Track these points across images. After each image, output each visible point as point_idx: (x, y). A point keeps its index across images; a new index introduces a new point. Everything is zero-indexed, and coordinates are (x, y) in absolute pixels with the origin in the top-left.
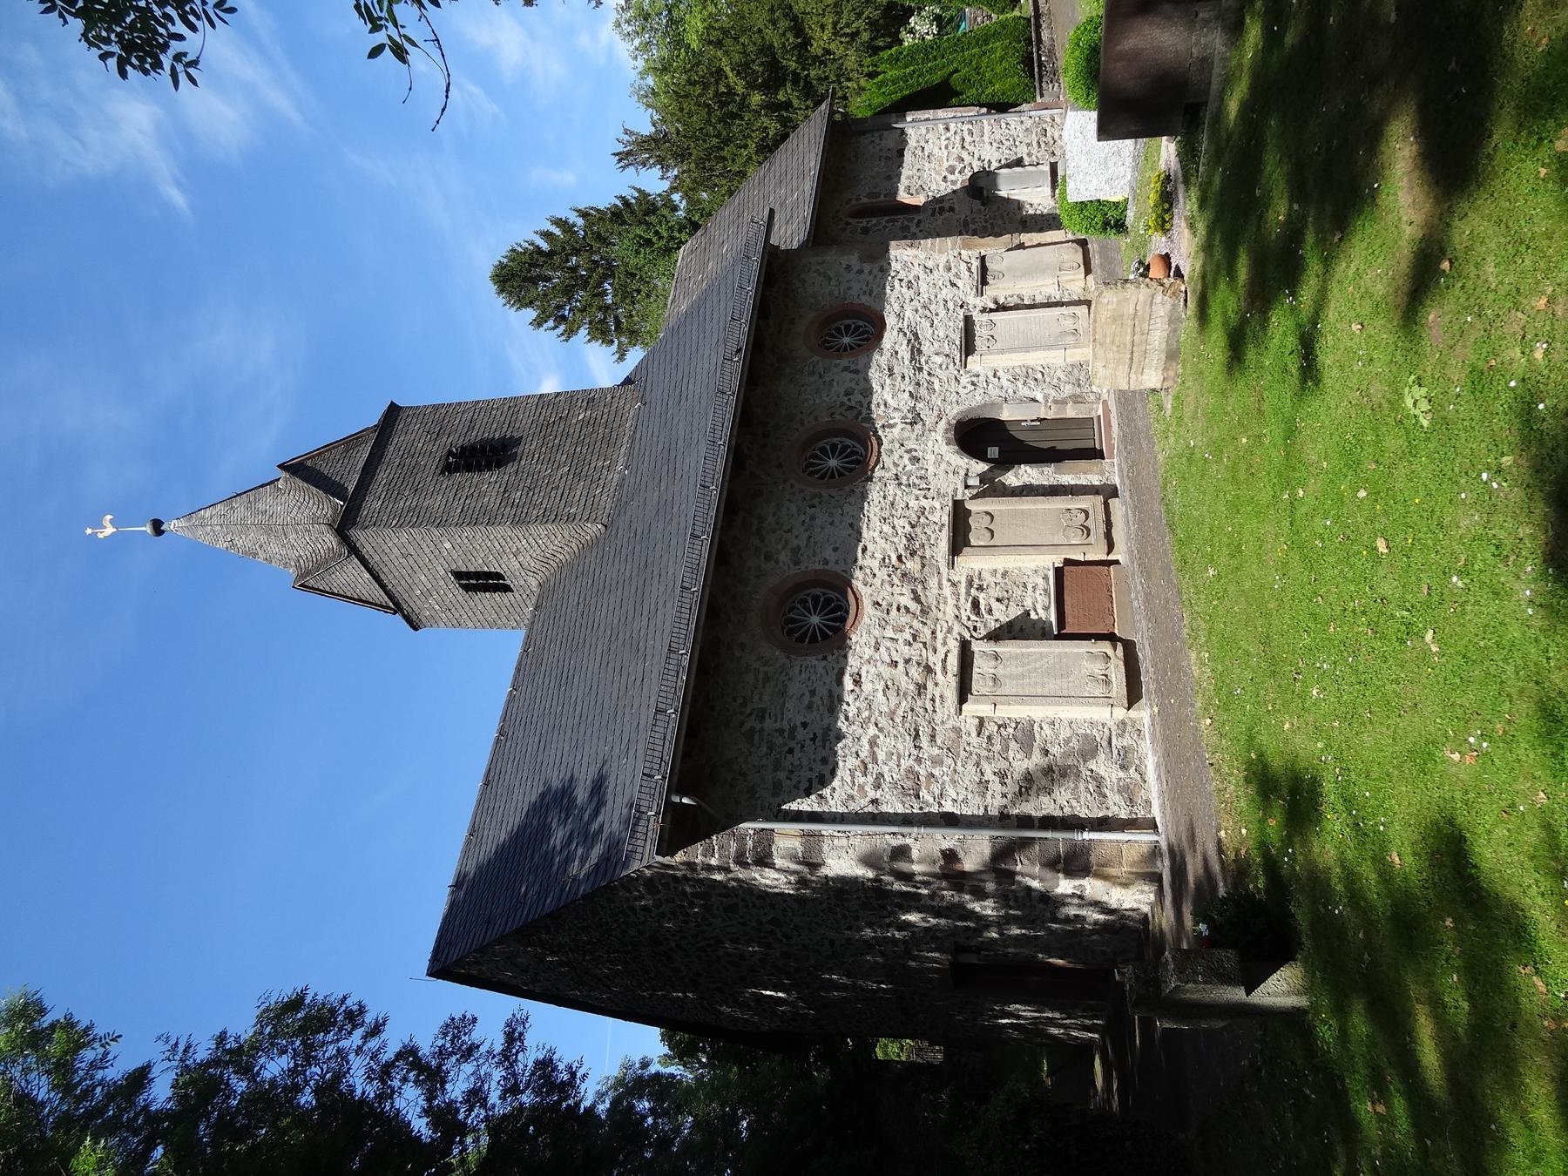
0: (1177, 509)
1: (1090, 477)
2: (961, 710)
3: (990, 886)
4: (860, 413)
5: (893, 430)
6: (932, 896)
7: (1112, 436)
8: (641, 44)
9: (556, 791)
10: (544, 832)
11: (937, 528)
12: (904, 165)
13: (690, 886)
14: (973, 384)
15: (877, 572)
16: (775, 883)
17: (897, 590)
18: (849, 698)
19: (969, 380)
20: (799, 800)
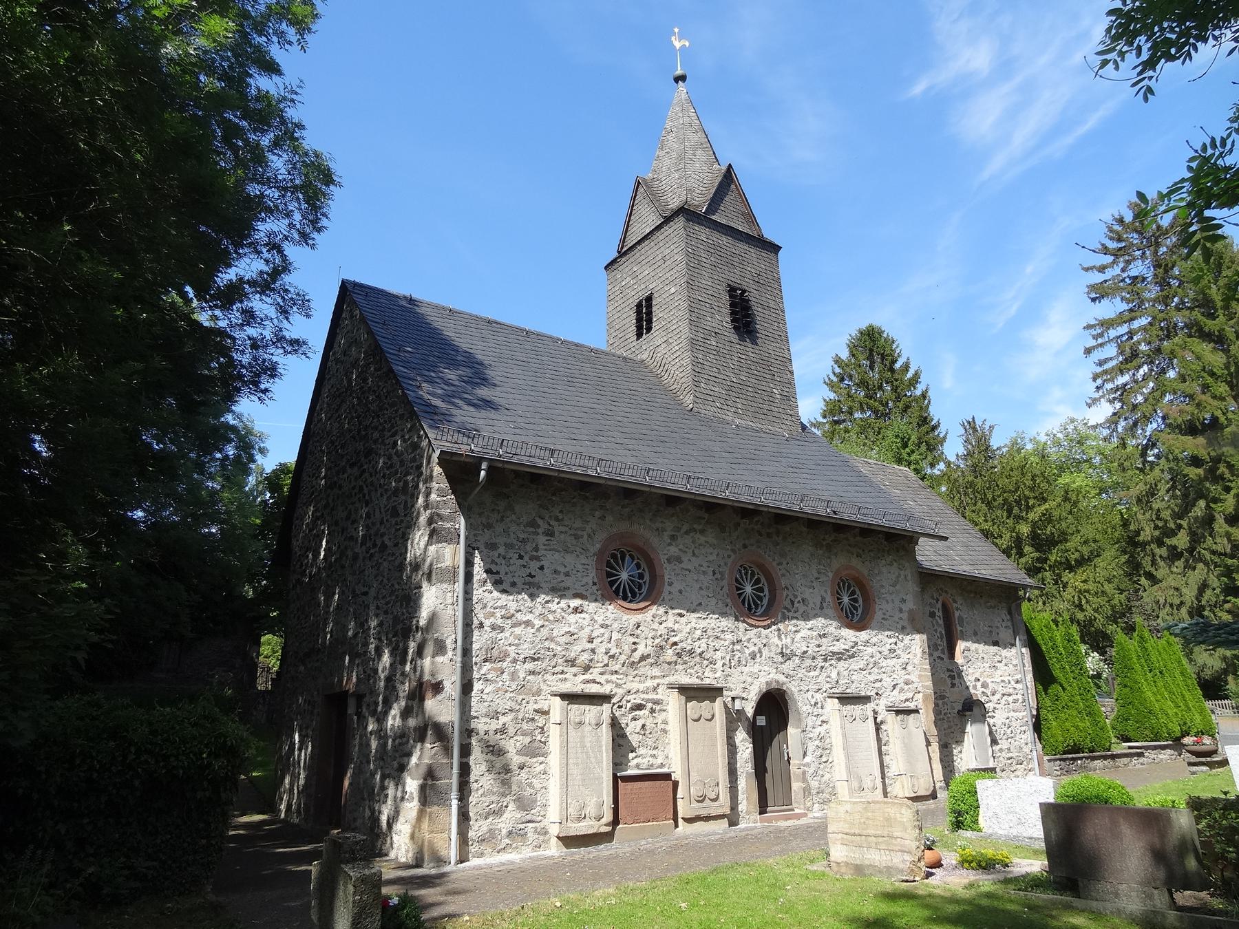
0: (731, 875)
1: (745, 802)
2: (555, 695)
3: (412, 722)
4: (789, 611)
5: (777, 638)
6: (403, 674)
7: (777, 821)
8: (1059, 439)
9: (485, 374)
10: (453, 364)
11: (699, 674)
12: (986, 647)
13: (413, 479)
14: (816, 704)
15: (664, 625)
16: (416, 547)
17: (649, 642)
18: (563, 603)
19: (819, 700)
20: (482, 564)
